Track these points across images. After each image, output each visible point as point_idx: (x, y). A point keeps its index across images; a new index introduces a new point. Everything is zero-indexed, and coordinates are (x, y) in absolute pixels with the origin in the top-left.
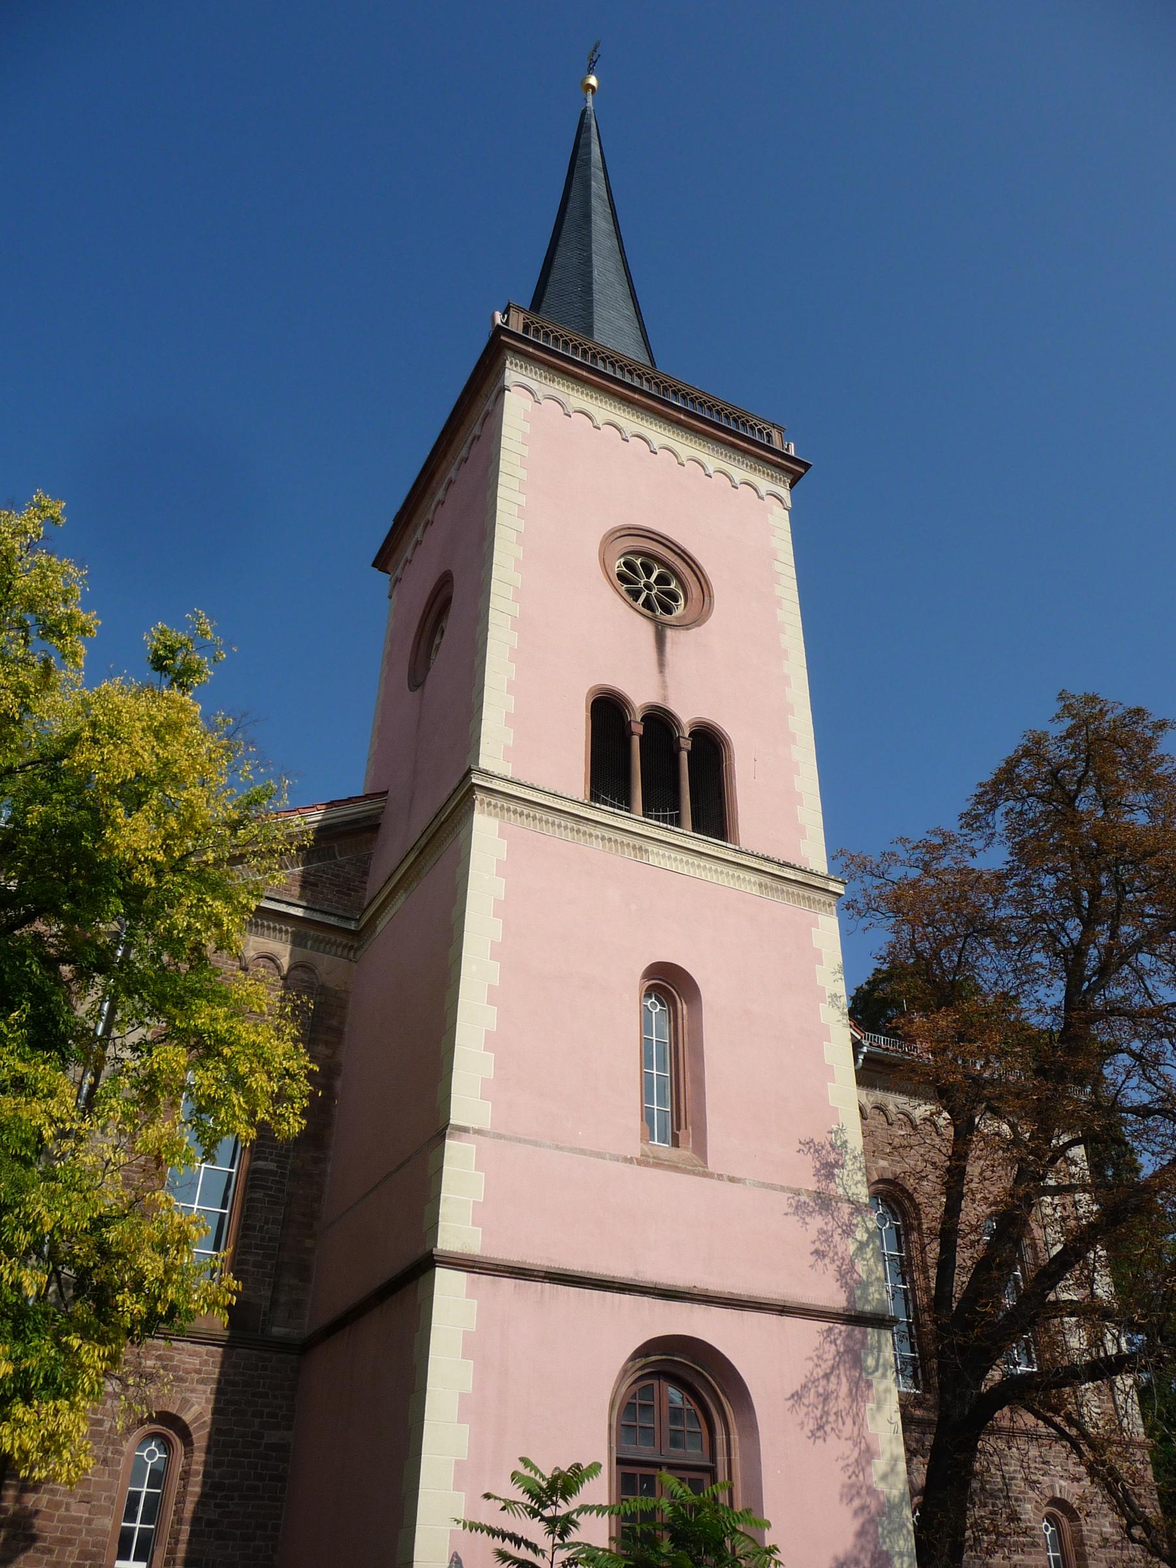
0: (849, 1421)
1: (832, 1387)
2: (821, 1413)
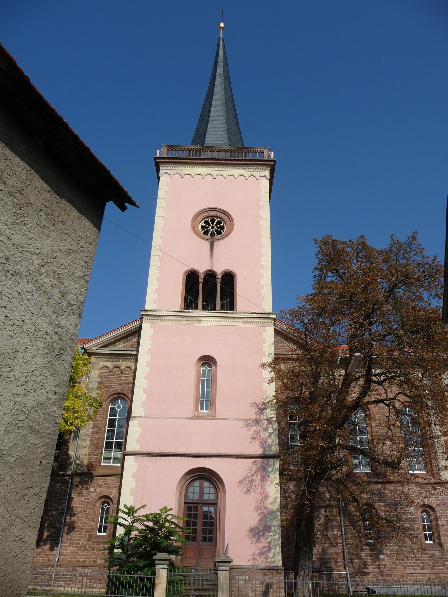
0: (260, 488)
1: (254, 478)
2: (248, 485)
